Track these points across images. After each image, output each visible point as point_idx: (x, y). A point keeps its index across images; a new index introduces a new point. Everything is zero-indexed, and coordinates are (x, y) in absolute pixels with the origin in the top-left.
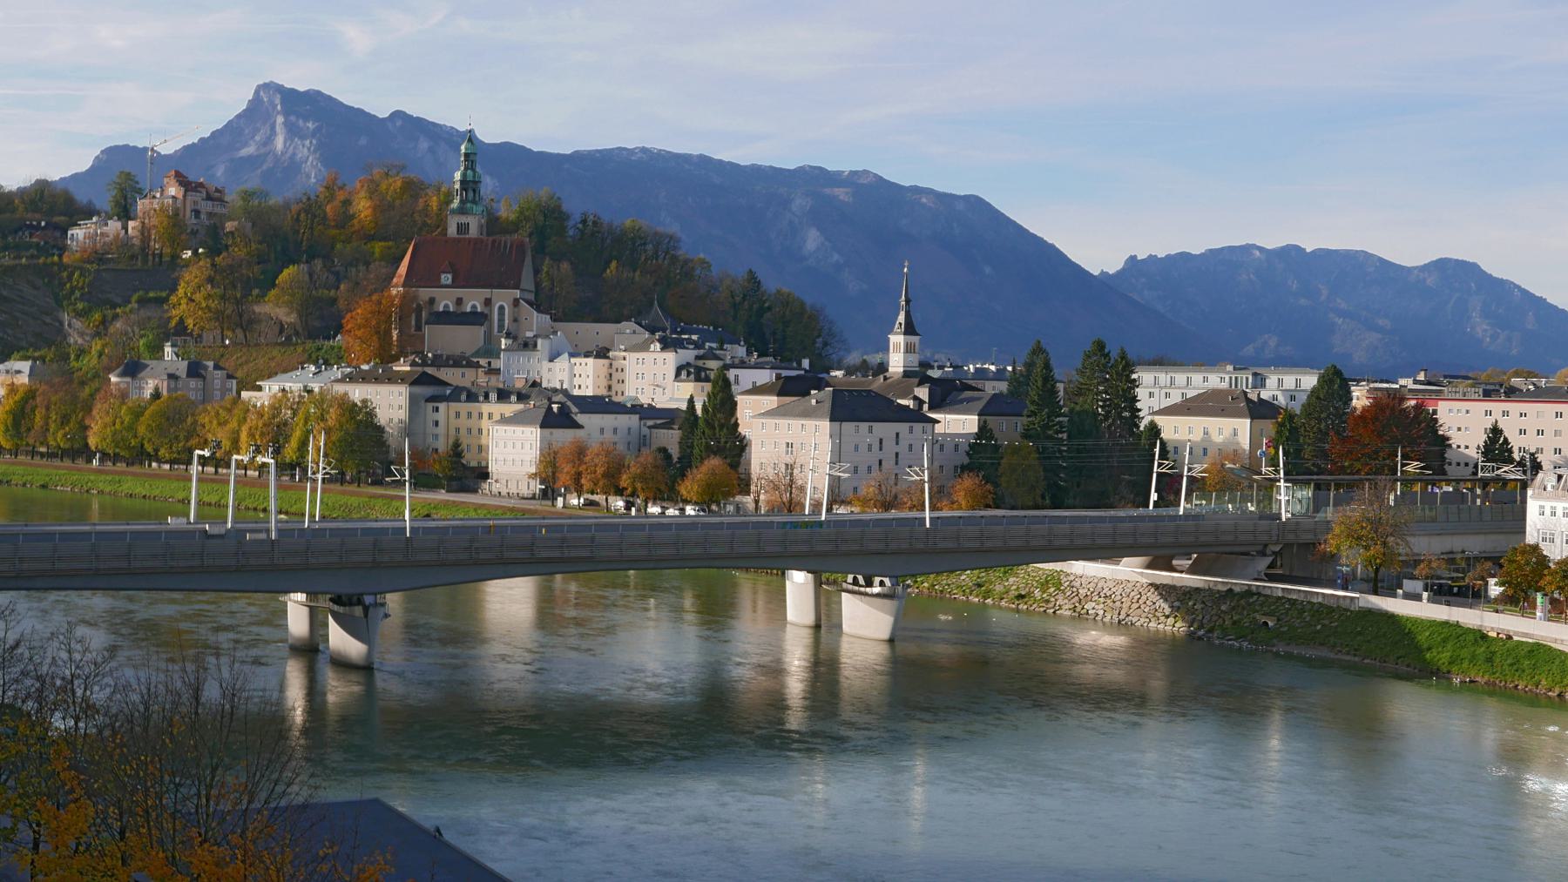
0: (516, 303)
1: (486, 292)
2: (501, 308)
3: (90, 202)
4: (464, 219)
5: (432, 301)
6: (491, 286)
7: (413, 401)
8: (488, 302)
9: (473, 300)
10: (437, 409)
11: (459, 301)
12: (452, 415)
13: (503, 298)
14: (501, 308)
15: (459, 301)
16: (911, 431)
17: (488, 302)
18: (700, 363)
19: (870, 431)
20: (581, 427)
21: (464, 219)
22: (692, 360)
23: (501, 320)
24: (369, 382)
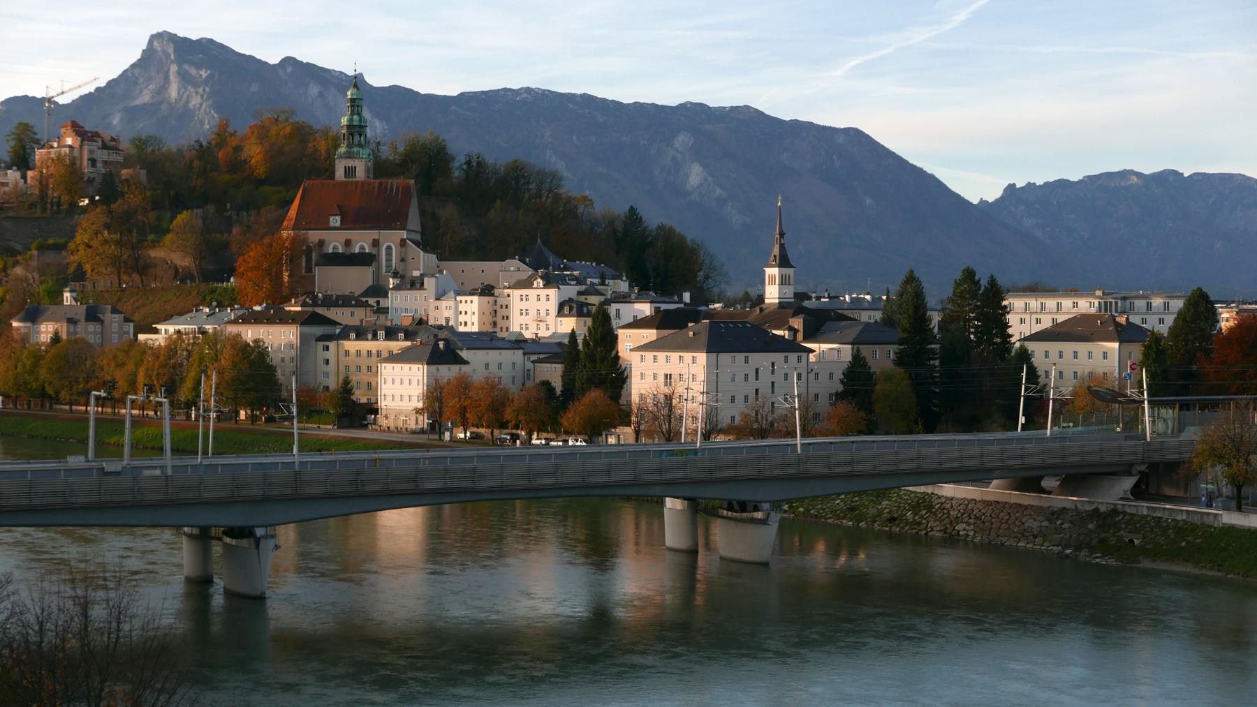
0: (403, 243)
1: (374, 234)
2: (389, 248)
4: (350, 163)
5: (321, 243)
7: (303, 338)
8: (376, 243)
9: (362, 241)
10: (327, 348)
11: (348, 243)
12: (1034, 321)
13: (391, 239)
14: (389, 248)
15: (348, 243)
16: (786, 360)
17: (376, 243)
18: (582, 298)
19: (747, 361)
20: (466, 363)
21: (350, 163)
22: (574, 296)
23: (389, 260)
24: (261, 323)
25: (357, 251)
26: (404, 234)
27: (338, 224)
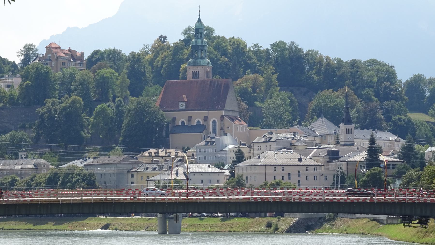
2: (214, 122)
3: (46, 47)
5: (174, 119)
6: (208, 109)
8: (206, 119)
9: (198, 117)
11: (190, 119)
14: (214, 122)
15: (190, 119)
17: (206, 119)
25: (195, 124)
26: (223, 113)
27: (184, 107)
